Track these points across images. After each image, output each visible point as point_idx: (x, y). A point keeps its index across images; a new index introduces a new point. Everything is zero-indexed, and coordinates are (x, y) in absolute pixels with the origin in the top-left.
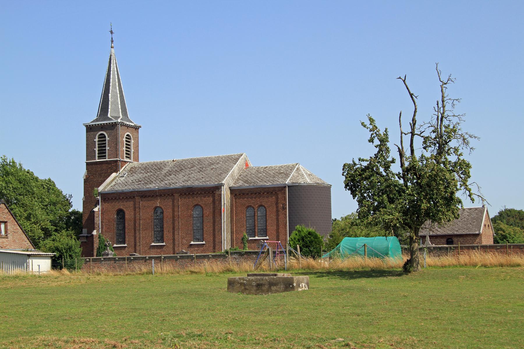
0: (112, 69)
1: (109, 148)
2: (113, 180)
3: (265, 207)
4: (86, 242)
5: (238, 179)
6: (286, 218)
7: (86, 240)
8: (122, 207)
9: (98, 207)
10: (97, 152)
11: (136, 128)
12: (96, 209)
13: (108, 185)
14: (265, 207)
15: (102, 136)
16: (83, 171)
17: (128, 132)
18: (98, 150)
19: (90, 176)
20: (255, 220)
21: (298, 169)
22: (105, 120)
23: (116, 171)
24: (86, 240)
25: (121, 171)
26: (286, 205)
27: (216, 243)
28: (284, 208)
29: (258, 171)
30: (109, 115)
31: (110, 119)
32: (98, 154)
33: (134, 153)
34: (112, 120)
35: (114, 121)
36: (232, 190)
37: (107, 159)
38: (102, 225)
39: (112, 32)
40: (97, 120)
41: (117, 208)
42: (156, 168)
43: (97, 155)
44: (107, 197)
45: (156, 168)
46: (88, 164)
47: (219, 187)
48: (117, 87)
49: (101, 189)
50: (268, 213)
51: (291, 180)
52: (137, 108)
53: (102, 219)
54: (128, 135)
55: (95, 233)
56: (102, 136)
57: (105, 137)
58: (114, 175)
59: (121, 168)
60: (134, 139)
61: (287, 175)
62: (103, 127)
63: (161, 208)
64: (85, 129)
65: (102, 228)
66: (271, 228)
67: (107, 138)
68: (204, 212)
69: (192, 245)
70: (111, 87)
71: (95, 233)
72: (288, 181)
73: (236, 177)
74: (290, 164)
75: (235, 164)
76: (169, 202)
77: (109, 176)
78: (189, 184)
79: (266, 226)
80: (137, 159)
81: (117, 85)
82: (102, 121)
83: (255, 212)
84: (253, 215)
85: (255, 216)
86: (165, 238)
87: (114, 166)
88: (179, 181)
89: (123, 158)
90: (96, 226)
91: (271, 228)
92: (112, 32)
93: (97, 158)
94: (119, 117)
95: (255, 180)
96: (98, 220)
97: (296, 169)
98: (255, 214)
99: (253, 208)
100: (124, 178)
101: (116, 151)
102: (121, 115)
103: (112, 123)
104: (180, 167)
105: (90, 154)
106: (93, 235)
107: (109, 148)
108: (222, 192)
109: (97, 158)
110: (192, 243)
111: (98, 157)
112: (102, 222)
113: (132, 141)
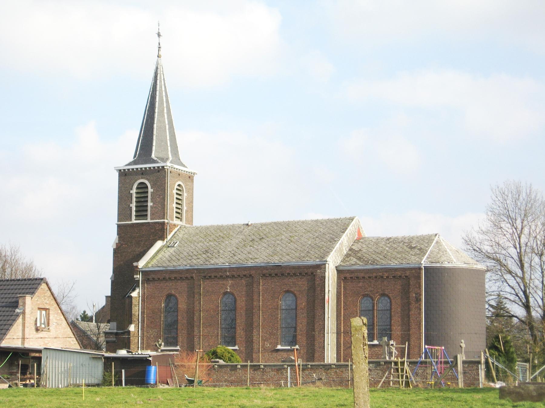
0: (158, 89)
1: (152, 204)
2: (158, 252)
3: (389, 298)
4: (114, 342)
5: (348, 256)
6: (420, 314)
7: (115, 339)
8: (166, 293)
9: (137, 291)
10: (134, 209)
11: (190, 177)
12: (134, 294)
13: (152, 259)
14: (389, 298)
15: (142, 187)
16: (111, 237)
17: (179, 180)
18: (136, 207)
19: (122, 245)
20: (374, 316)
21: (437, 242)
22: (146, 163)
23: (162, 238)
24: (115, 339)
25: (169, 237)
26: (420, 295)
27: (313, 350)
28: (418, 300)
29: (378, 241)
30: (153, 156)
31: (154, 162)
32: (136, 211)
33: (187, 211)
34: (158, 162)
35: (160, 164)
36: (340, 271)
37: (149, 220)
38: (143, 317)
39: (159, 35)
40: (134, 163)
41: (166, 293)
42: (222, 235)
43: (134, 213)
44: (150, 276)
45: (220, 233)
46: (119, 226)
47: (321, 267)
48: (166, 115)
49: (141, 264)
50: (393, 307)
51: (428, 258)
52: (191, 148)
53: (143, 308)
54: (179, 185)
55: (132, 328)
56: (142, 187)
57: (147, 187)
58: (159, 244)
59: (169, 234)
60: (187, 192)
61: (422, 252)
62: (143, 173)
63: (233, 294)
64: (117, 174)
65: (143, 321)
66: (397, 330)
67: (150, 190)
68: (299, 302)
69: (278, 350)
70: (156, 115)
71: (132, 328)
72: (424, 262)
73: (345, 252)
74: (431, 233)
75: (344, 232)
76: (183, 286)
77: (151, 245)
78: (276, 260)
79: (391, 325)
80: (190, 220)
81: (165, 111)
82: (142, 164)
83: (374, 304)
84: (371, 308)
85: (373, 309)
86: (238, 339)
87: (159, 231)
88: (261, 256)
89: (173, 220)
90: (134, 319)
91: (397, 330)
92: (159, 35)
93: (134, 217)
94: (167, 159)
95: (374, 256)
96: (137, 310)
97: (435, 242)
98: (373, 307)
99: (372, 298)
100: (173, 249)
101: (162, 211)
102: (170, 156)
103: (158, 167)
104: (258, 233)
105: (123, 212)
106: (129, 332)
107: (152, 204)
108: (327, 274)
109: (134, 217)
110: (279, 347)
111: (136, 216)
112: (143, 313)
113: (185, 194)
